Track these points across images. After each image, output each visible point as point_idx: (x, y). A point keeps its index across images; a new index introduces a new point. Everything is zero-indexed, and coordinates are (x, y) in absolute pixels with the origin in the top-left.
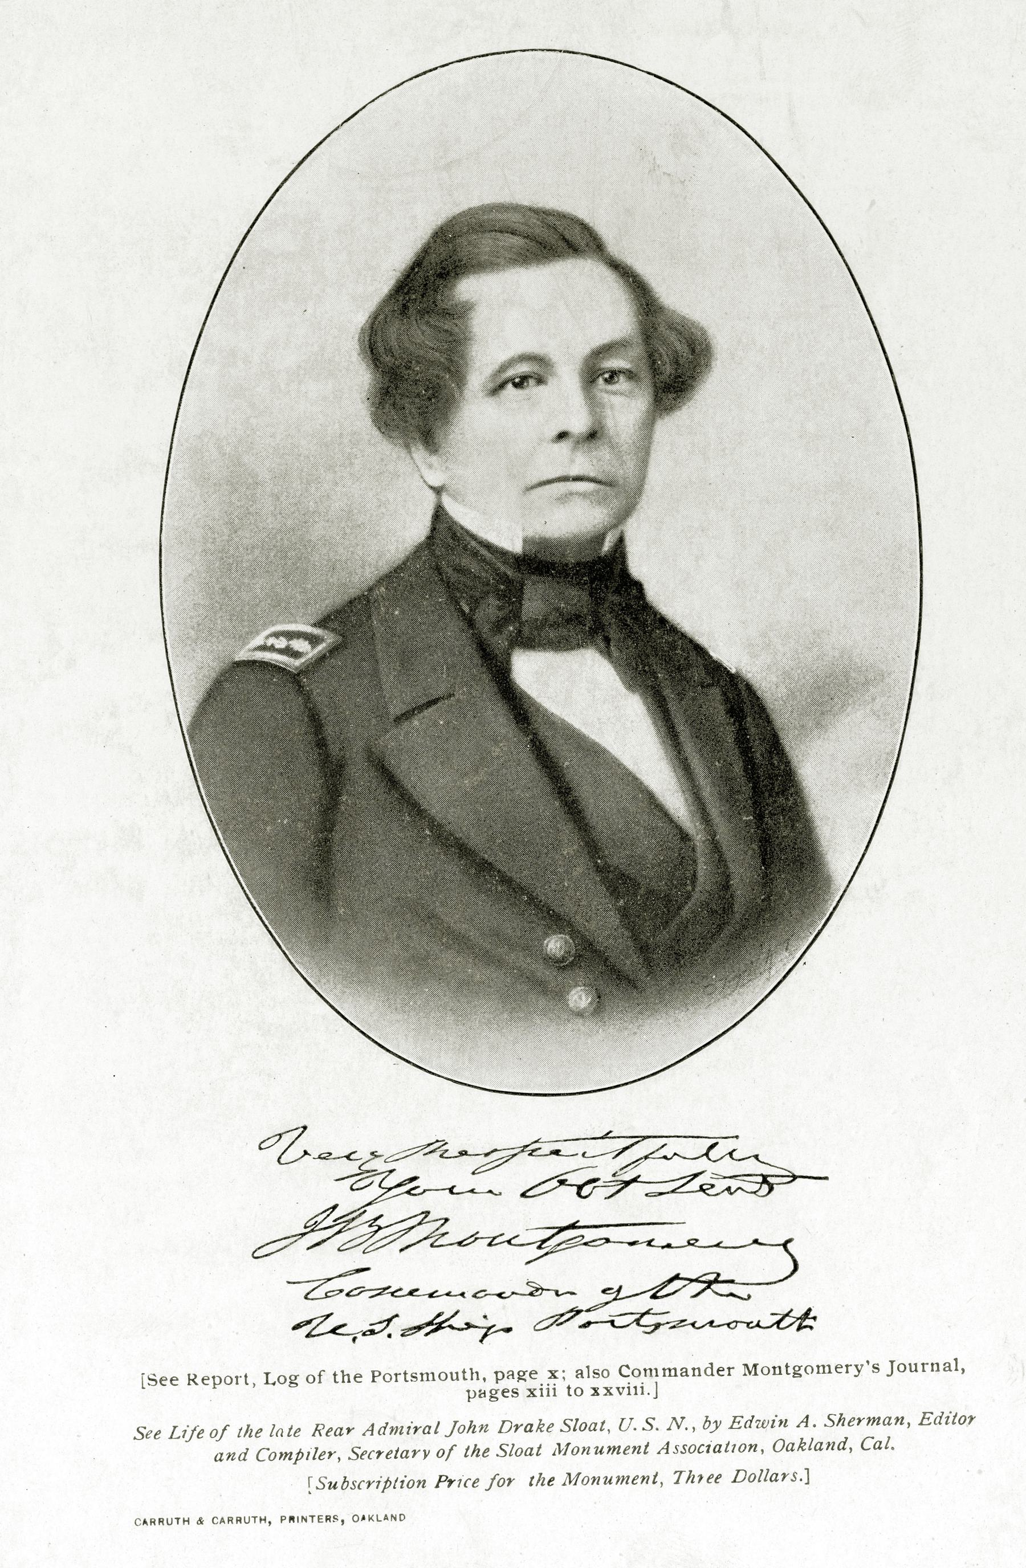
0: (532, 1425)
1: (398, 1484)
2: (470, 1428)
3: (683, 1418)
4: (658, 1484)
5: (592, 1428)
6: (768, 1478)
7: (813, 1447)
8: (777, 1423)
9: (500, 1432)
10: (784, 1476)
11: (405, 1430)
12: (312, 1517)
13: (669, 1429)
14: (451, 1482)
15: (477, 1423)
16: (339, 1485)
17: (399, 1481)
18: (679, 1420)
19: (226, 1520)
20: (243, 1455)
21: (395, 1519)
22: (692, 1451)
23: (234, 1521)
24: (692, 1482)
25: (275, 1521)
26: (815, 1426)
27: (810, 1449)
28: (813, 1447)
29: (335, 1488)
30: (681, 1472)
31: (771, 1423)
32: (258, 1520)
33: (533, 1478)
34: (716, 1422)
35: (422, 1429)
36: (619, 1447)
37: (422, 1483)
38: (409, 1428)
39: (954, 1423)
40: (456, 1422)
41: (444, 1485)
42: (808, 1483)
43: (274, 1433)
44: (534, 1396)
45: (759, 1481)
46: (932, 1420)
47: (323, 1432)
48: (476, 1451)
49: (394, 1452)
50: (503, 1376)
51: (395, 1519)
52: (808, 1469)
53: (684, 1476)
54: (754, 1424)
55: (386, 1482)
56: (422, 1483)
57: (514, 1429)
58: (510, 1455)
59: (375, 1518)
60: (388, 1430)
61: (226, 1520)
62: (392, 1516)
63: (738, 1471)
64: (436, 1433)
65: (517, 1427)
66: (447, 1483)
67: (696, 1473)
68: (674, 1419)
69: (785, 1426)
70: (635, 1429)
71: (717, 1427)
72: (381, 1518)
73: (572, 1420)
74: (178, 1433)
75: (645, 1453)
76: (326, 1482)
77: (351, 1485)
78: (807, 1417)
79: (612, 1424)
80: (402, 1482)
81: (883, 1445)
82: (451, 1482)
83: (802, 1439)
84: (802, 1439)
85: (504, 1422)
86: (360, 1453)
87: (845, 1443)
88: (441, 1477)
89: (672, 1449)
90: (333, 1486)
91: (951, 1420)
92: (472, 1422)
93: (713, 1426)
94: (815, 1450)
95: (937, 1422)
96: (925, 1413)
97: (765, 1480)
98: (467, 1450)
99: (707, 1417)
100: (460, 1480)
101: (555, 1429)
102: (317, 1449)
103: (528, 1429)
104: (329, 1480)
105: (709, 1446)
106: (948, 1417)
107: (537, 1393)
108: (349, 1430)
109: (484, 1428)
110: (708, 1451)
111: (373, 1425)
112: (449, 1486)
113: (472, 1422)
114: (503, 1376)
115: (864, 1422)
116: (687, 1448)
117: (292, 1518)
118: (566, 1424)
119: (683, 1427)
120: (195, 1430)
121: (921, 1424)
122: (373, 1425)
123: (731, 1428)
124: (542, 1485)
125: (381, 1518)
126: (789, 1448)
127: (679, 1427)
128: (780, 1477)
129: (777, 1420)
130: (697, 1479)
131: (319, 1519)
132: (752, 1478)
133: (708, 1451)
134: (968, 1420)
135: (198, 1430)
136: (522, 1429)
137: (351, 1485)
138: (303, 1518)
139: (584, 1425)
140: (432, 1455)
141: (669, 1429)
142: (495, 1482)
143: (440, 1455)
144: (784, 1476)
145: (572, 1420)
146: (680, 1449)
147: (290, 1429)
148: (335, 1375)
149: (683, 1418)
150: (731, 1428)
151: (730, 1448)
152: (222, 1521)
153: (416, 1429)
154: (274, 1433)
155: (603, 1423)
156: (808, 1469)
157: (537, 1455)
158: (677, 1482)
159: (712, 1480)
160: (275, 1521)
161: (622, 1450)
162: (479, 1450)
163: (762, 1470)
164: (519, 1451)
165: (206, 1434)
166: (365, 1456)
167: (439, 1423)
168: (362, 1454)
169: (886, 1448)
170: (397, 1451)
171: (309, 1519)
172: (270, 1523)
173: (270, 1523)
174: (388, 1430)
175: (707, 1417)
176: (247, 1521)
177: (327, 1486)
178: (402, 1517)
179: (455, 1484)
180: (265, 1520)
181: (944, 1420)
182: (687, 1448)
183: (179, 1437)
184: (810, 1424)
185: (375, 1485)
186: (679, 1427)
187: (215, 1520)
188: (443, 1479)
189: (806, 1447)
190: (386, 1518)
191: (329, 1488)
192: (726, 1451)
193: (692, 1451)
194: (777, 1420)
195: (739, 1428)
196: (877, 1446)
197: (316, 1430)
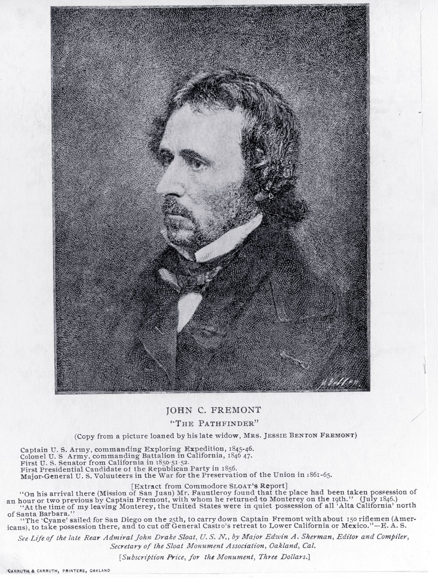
0: (168, 537)
1: (153, 558)
2: (144, 537)
3: (225, 535)
4: (253, 559)
5: (190, 538)
6: (295, 557)
7: (285, 546)
8: (284, 537)
9: (156, 539)
10: (269, 557)
11: (120, 538)
12: (75, 570)
13: (219, 539)
14: (173, 557)
15: (147, 536)
16: (131, 558)
17: (154, 556)
18: (223, 536)
19: (42, 571)
20: (296, 546)
21: (106, 571)
22: (239, 547)
23: (45, 571)
24: (266, 559)
25: (61, 571)
26: (298, 538)
27: (283, 547)
28: (285, 546)
29: (129, 559)
30: (262, 555)
31: (281, 537)
32: (54, 571)
33: (206, 556)
34: (237, 536)
35: (164, 537)
36: (212, 545)
37: (162, 558)
38: (121, 537)
39: (76, 539)
40: (139, 535)
41: (170, 558)
42: (309, 560)
43: (70, 538)
44: (355, 527)
45: (291, 559)
46: (342, 537)
47: (89, 538)
48: (159, 546)
49: (128, 546)
50: (55, 514)
51: (106, 571)
52: (309, 554)
53: (263, 556)
54: (275, 537)
55: (149, 557)
56: (162, 558)
57: (161, 538)
58: (171, 548)
59: (98, 571)
60: (113, 538)
61: (42, 571)
62: (105, 570)
63: (284, 555)
64: (131, 539)
65: (162, 537)
66: (172, 558)
67: (268, 555)
68: (221, 535)
69: (287, 538)
70: (206, 539)
71: (238, 538)
72: (101, 570)
73: (183, 535)
74: (34, 538)
75: (222, 548)
76: (126, 557)
77: (135, 558)
78: (295, 535)
79: (198, 537)
80: (155, 557)
81: (311, 546)
82: (173, 557)
83: (281, 543)
84: (281, 543)
85: (157, 535)
86: (115, 546)
87: (297, 545)
88: (169, 555)
89: (232, 546)
90: (129, 558)
91: (349, 537)
92: (145, 535)
93: (236, 538)
94: (286, 548)
95: (344, 538)
96: (339, 535)
97: (294, 558)
98: (155, 545)
99: (234, 534)
100: (177, 557)
101: (177, 538)
102: (284, 543)
103: (128, 538)
104: (127, 556)
105: (246, 545)
106: (348, 536)
107: (357, 526)
108: (98, 538)
109: (150, 538)
110: (245, 547)
111: (107, 536)
112: (172, 559)
113: (145, 535)
114: (55, 514)
115: (317, 537)
116: (237, 546)
117: (67, 570)
118: (180, 536)
119: (225, 538)
120: (41, 537)
121: (338, 538)
122: (107, 536)
123: (267, 538)
124: (210, 559)
125: (101, 570)
126: (276, 547)
127: (223, 538)
128: (299, 557)
129: (284, 536)
130: (268, 557)
131: (77, 571)
132: (288, 557)
133: (245, 547)
134: (260, 537)
135: (42, 537)
136: (164, 538)
137: (135, 558)
138: (71, 570)
139: (187, 537)
140: (142, 547)
141: (219, 539)
142: (192, 557)
143: (145, 547)
144: (301, 557)
145: (183, 535)
146: (235, 546)
147: (76, 537)
148: (156, 519)
149: (225, 535)
150: (267, 538)
151: (254, 546)
152: (41, 571)
153: (124, 538)
154: (70, 538)
155: (194, 536)
156: (309, 554)
157: (182, 548)
158: (261, 559)
159: (274, 558)
160: (61, 571)
161: (213, 546)
162: (160, 546)
163: (292, 555)
164: (175, 546)
165: (45, 539)
166: (117, 547)
167: (132, 535)
168: (116, 547)
169: (312, 547)
170: (129, 546)
171: (74, 571)
172: (58, 572)
173: (58, 572)
174: (113, 538)
175: (234, 534)
176: (50, 571)
177: (126, 558)
178: (109, 570)
179: (175, 558)
180: (57, 571)
181: (346, 537)
182: (237, 546)
183: (35, 540)
184: (296, 537)
185: (144, 558)
186: (223, 538)
187: (38, 571)
188: (170, 556)
189: (282, 546)
190: (102, 571)
191: (127, 559)
192: (252, 547)
193: (239, 547)
194: (284, 536)
195: (341, 539)
196: (309, 547)
197: (86, 537)
